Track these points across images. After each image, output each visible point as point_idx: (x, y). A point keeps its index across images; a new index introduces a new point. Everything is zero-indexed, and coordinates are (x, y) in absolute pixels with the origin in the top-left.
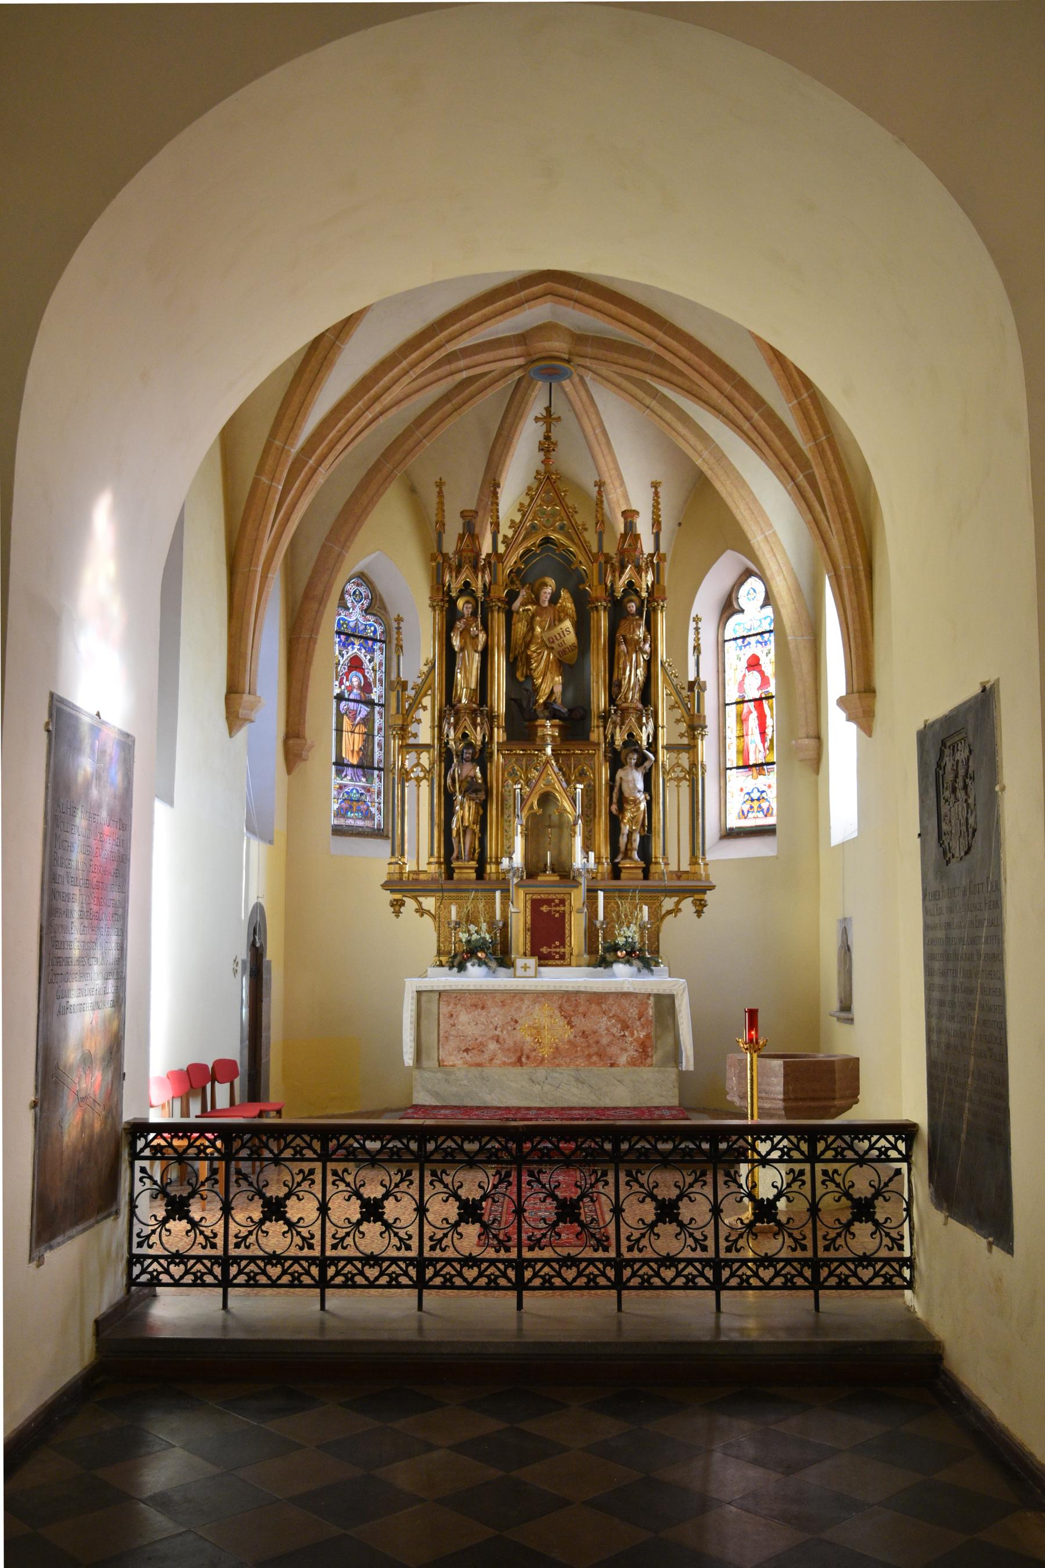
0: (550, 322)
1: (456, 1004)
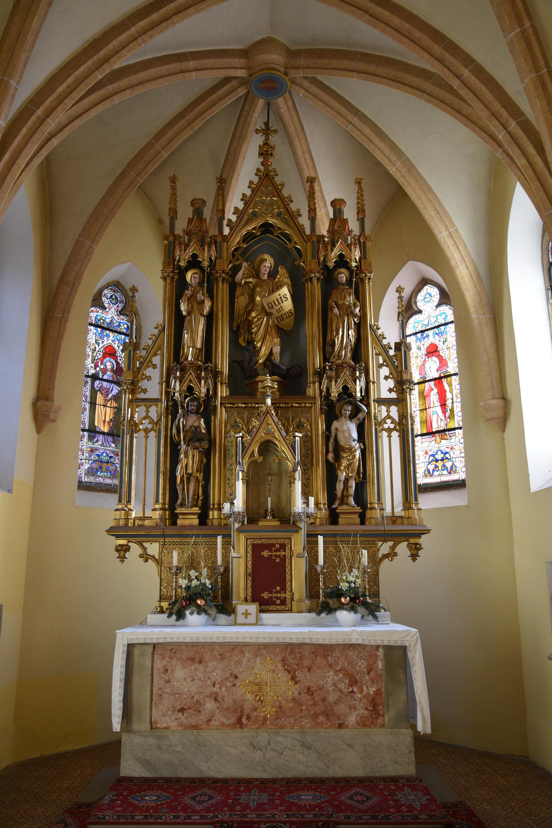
0: (269, 37)
1: (171, 658)
